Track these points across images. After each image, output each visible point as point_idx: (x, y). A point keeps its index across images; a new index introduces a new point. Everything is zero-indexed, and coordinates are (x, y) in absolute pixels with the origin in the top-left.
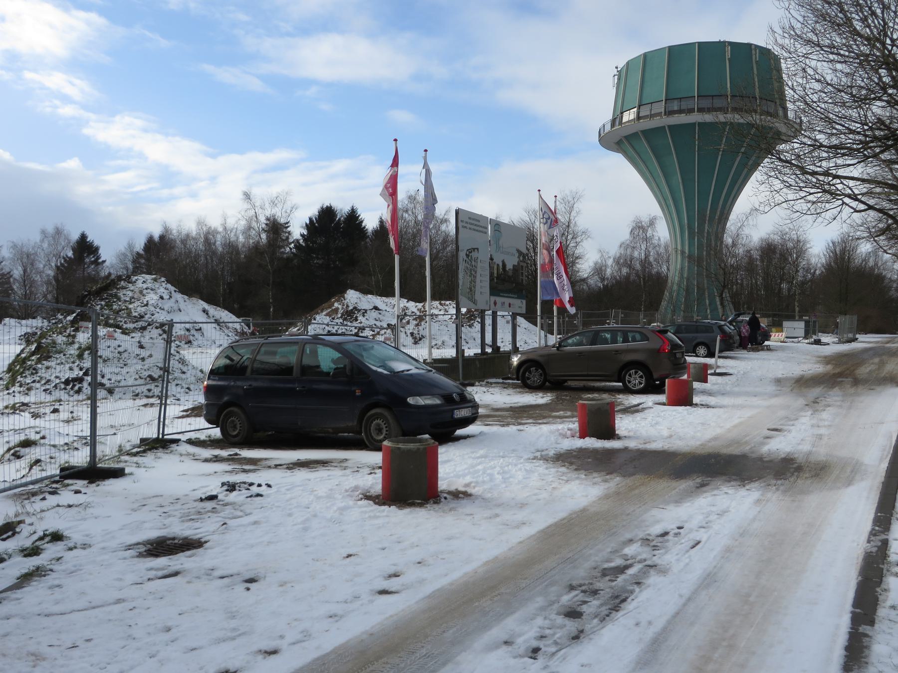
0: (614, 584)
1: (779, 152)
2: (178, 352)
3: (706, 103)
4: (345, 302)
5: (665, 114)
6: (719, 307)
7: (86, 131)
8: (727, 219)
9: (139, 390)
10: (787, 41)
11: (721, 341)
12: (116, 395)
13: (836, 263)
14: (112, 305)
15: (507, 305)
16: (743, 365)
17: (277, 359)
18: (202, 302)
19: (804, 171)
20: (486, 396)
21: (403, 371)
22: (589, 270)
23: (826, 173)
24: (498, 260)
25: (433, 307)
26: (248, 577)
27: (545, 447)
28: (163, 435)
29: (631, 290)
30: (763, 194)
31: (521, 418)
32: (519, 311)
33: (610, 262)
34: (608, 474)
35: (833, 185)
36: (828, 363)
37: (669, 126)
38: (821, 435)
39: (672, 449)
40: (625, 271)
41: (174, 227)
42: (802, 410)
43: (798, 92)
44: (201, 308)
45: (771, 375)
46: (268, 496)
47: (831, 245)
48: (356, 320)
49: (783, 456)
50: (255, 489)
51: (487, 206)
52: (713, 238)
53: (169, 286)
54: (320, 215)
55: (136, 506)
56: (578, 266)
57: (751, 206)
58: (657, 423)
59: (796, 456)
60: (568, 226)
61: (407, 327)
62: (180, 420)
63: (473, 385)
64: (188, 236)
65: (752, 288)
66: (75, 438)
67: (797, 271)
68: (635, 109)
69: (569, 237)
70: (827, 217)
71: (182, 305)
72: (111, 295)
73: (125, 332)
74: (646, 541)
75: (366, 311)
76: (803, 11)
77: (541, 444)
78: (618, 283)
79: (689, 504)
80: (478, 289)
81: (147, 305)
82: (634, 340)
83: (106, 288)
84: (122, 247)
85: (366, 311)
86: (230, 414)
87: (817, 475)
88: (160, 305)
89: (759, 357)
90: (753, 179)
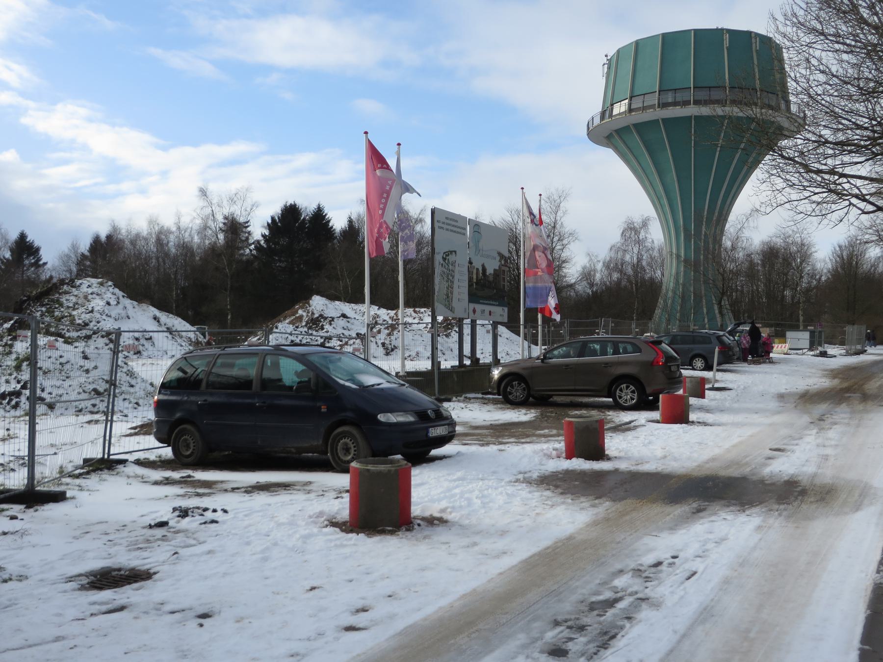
0: (602, 619)
2: (126, 364)
3: (703, 95)
4: (311, 309)
5: (659, 107)
6: (718, 315)
7: (24, 121)
8: (726, 220)
9: (82, 405)
10: (789, 29)
11: (719, 353)
12: (57, 411)
13: (843, 269)
14: (53, 312)
15: (487, 313)
16: (744, 379)
17: (235, 372)
19: (808, 170)
20: (465, 412)
21: (373, 386)
22: (576, 275)
23: (832, 172)
24: (478, 264)
25: (407, 314)
26: (201, 611)
27: (527, 469)
28: (109, 455)
29: (623, 297)
30: (764, 194)
31: (503, 436)
32: (500, 320)
33: (599, 266)
34: (597, 498)
35: (840, 184)
36: (834, 377)
37: (663, 119)
38: (827, 455)
40: (615, 276)
41: (123, 226)
42: (806, 428)
44: (151, 314)
47: (838, 249)
48: (322, 329)
49: (786, 478)
50: (209, 515)
51: (464, 204)
52: (711, 241)
53: (117, 291)
54: (282, 214)
55: (78, 533)
57: (751, 207)
58: (650, 443)
59: (800, 478)
60: (554, 227)
62: (128, 438)
63: (449, 400)
64: (138, 236)
65: (753, 296)
66: (12, 458)
67: (801, 277)
68: (627, 101)
71: (131, 312)
72: (53, 301)
73: (68, 341)
74: (638, 572)
75: (333, 319)
77: (525, 465)
79: (684, 531)
81: (92, 311)
82: (625, 352)
84: (65, 247)
85: (333, 319)
87: (822, 499)
88: (107, 311)
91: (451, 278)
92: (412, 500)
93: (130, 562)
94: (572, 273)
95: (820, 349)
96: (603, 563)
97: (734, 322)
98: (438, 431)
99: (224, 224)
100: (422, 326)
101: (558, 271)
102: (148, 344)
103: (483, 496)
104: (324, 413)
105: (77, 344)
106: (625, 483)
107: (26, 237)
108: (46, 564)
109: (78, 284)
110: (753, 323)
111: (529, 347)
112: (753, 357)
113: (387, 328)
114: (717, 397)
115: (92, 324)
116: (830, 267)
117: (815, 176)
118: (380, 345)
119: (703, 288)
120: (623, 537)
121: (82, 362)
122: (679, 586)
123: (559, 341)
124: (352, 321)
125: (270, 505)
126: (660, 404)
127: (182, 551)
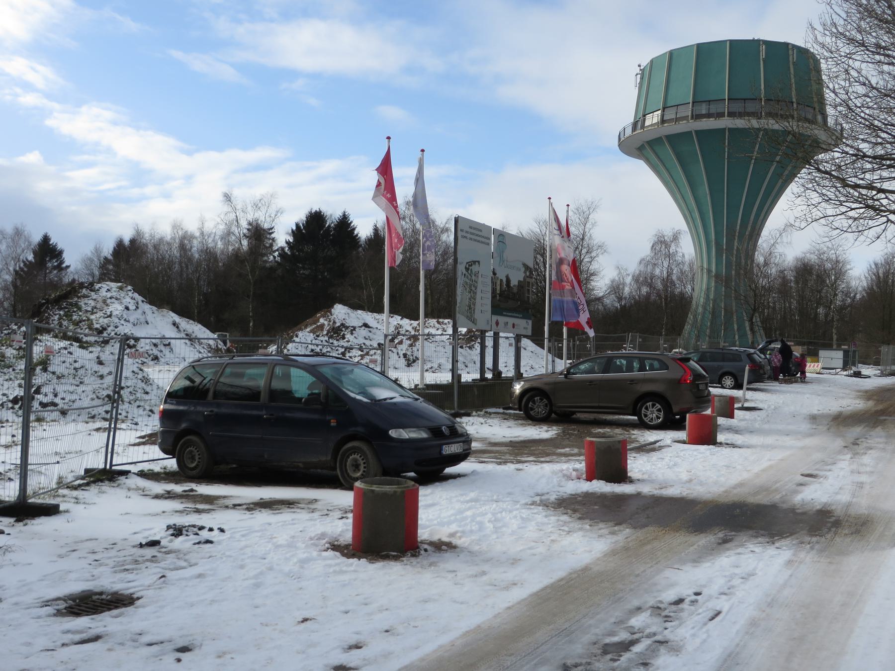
0: (616, 664)
1: (816, 162)
2: (141, 370)
3: (738, 107)
4: (332, 318)
5: (692, 118)
6: (749, 332)
7: (49, 122)
8: (759, 235)
9: (94, 412)
10: (828, 39)
11: (750, 371)
12: (70, 417)
13: (878, 287)
14: (72, 316)
15: (510, 325)
16: (775, 398)
17: (245, 382)
18: (173, 314)
19: (845, 185)
20: (481, 428)
21: (385, 399)
22: (604, 289)
23: (870, 187)
24: (501, 275)
25: (433, 326)
26: (181, 644)
27: (545, 491)
28: (111, 465)
29: (652, 311)
30: (799, 208)
31: (521, 454)
32: (524, 332)
33: (628, 280)
34: (616, 525)
35: (878, 200)
36: (869, 399)
37: (696, 132)
38: (862, 483)
39: (692, 496)
40: (645, 290)
41: (146, 230)
42: (840, 452)
43: (840, 96)
44: (171, 320)
45: (806, 411)
46: (220, 542)
47: (873, 267)
48: (343, 338)
49: (818, 507)
50: (205, 534)
51: (489, 214)
52: (743, 256)
53: (136, 295)
54: (307, 221)
55: (63, 551)
56: (593, 283)
57: (785, 221)
58: (675, 465)
59: (833, 508)
60: (583, 239)
61: (400, 347)
62: (136, 448)
63: (469, 415)
64: (161, 240)
65: (785, 313)
66: (12, 467)
67: (836, 295)
68: (659, 112)
69: (584, 251)
70: (870, 236)
71: (150, 317)
72: (71, 304)
73: (83, 346)
74: (657, 609)
75: (354, 328)
76: (846, 6)
77: (541, 487)
78: (637, 303)
79: (708, 564)
80: (478, 308)
81: (110, 316)
82: (652, 368)
83: (65, 296)
84: (87, 250)
85: (354, 328)
86: (189, 444)
87: (857, 532)
88: (125, 316)
89: (790, 389)
90: (788, 191)
91: (473, 288)
92: (419, 522)
93: (114, 586)
94: (601, 285)
95: (854, 369)
96: (620, 599)
97: (765, 340)
98: (452, 449)
99: (248, 230)
100: (445, 338)
101: (586, 284)
102: (166, 351)
103: (496, 520)
104: (334, 427)
105: (90, 349)
106: (648, 508)
107: (50, 240)
108: (24, 585)
109: (97, 287)
110: (782, 342)
111: (553, 361)
112: (784, 376)
113: (409, 339)
114: (747, 417)
115: (109, 329)
116: (865, 285)
117: (852, 191)
118: (402, 356)
119: (734, 304)
120: (642, 569)
121: (97, 367)
122: (701, 628)
123: (586, 356)
124: (374, 331)
125: (270, 524)
126: (687, 423)
127: (169, 574)
